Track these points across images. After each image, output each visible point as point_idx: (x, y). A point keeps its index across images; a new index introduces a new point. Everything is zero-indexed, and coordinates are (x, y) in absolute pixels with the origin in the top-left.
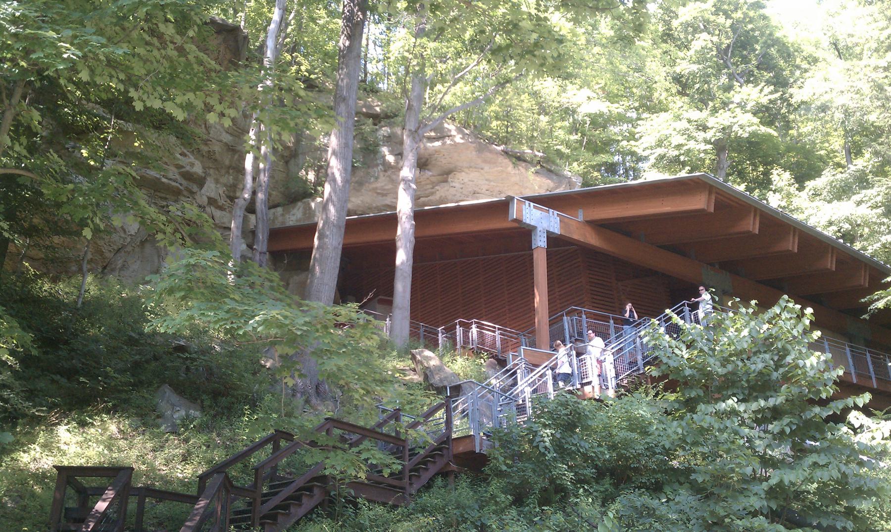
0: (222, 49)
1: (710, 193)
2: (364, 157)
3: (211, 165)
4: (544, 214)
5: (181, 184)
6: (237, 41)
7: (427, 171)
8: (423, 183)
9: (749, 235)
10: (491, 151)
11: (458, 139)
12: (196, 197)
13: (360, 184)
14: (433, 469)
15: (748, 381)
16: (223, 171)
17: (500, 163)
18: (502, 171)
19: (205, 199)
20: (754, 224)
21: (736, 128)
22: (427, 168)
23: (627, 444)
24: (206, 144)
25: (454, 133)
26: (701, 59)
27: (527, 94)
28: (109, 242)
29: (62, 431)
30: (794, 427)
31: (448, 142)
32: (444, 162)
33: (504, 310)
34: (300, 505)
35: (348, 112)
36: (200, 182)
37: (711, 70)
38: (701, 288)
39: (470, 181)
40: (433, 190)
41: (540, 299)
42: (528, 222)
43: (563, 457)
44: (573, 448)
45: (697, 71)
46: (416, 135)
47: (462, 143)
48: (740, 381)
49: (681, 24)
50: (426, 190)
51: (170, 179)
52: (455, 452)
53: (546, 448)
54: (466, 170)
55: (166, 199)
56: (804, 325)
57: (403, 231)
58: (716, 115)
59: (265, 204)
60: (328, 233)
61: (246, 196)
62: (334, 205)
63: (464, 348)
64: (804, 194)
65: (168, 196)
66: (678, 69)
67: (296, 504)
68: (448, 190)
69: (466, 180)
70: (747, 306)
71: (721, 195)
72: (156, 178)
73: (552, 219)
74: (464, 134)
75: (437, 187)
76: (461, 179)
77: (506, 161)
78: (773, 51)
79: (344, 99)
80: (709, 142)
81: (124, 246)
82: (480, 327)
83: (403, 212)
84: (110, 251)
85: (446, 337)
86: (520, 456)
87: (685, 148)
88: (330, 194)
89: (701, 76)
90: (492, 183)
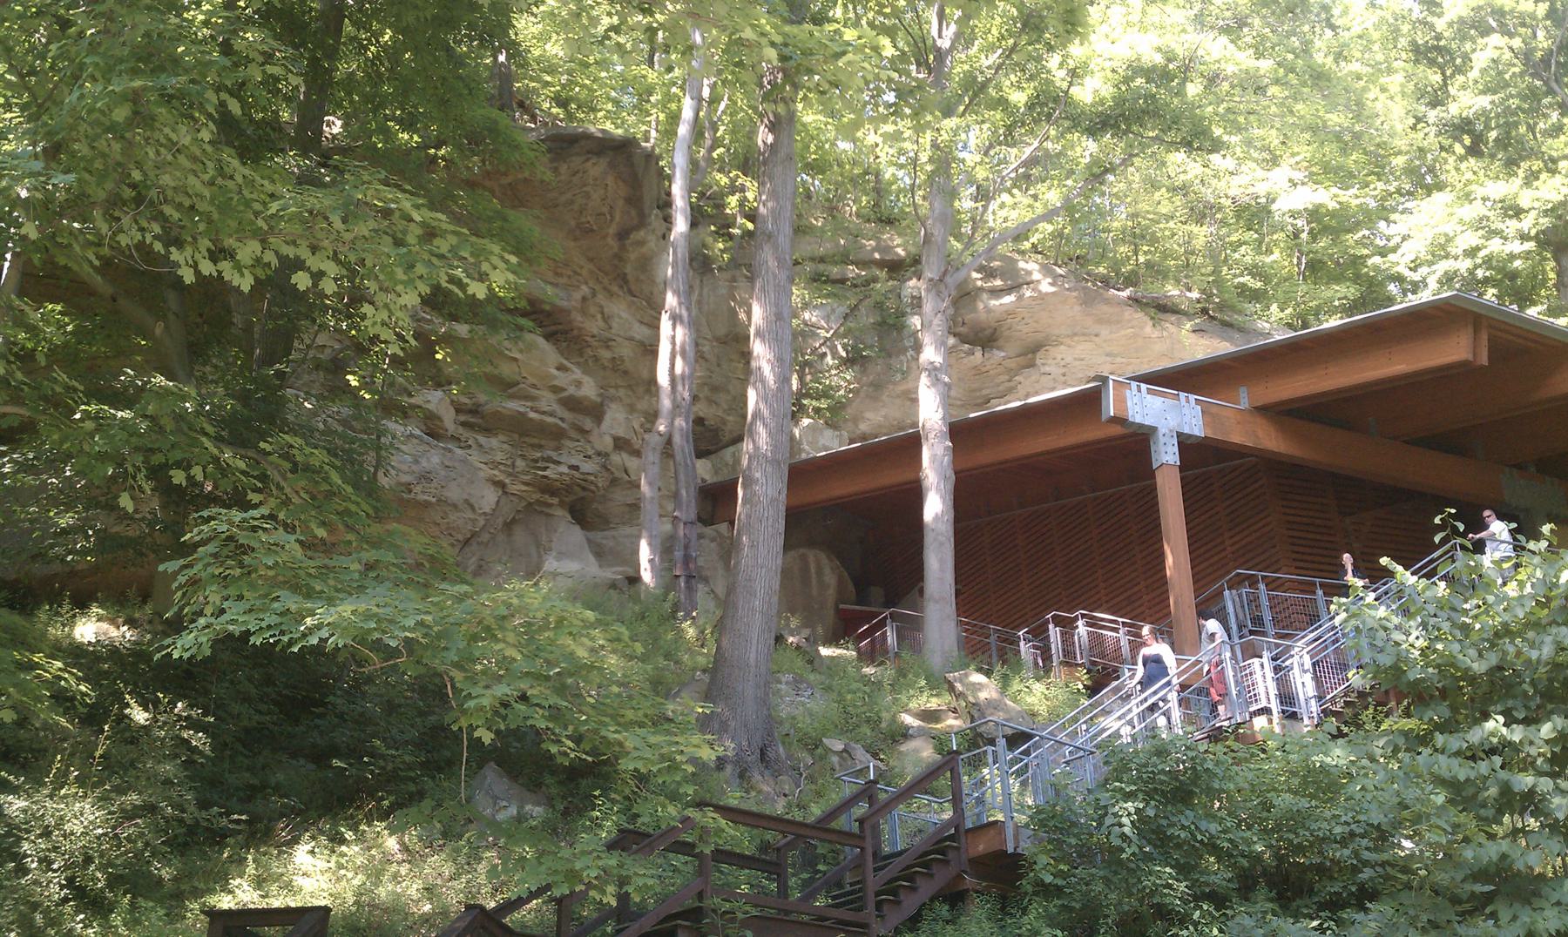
1: (1476, 332)
2: (880, 338)
3: (619, 382)
4: (1169, 402)
5: (562, 419)
7: (995, 352)
10: (1107, 301)
11: (1046, 286)
12: (591, 439)
13: (877, 386)
14: (926, 889)
15: (1533, 683)
16: (641, 390)
17: (1129, 321)
18: (1135, 336)
19: (609, 441)
22: (995, 344)
23: (1297, 819)
24: (608, 347)
25: (1036, 276)
26: (1495, 83)
27: (1164, 190)
28: (448, 529)
31: (1028, 294)
32: (1025, 331)
36: (596, 412)
38: (1487, 513)
40: (1012, 384)
41: (1175, 559)
42: (1138, 419)
43: (1166, 852)
45: (1489, 107)
46: (942, 287)
47: (1053, 293)
48: (1520, 684)
49: (1450, 25)
50: (998, 385)
51: (544, 413)
53: (1124, 836)
54: (1068, 341)
55: (540, 447)
58: (1536, 184)
60: (758, 475)
61: (662, 428)
62: (765, 426)
65: (543, 442)
66: (1454, 110)
69: (1069, 359)
72: (520, 413)
73: (1186, 411)
74: (1056, 277)
76: (1059, 357)
77: (1140, 316)
79: (770, 236)
80: (1524, 237)
81: (474, 534)
82: (1093, 623)
85: (1034, 647)
86: (1086, 854)
87: (1482, 254)
88: (757, 403)
89: (1498, 116)
90: (1119, 360)
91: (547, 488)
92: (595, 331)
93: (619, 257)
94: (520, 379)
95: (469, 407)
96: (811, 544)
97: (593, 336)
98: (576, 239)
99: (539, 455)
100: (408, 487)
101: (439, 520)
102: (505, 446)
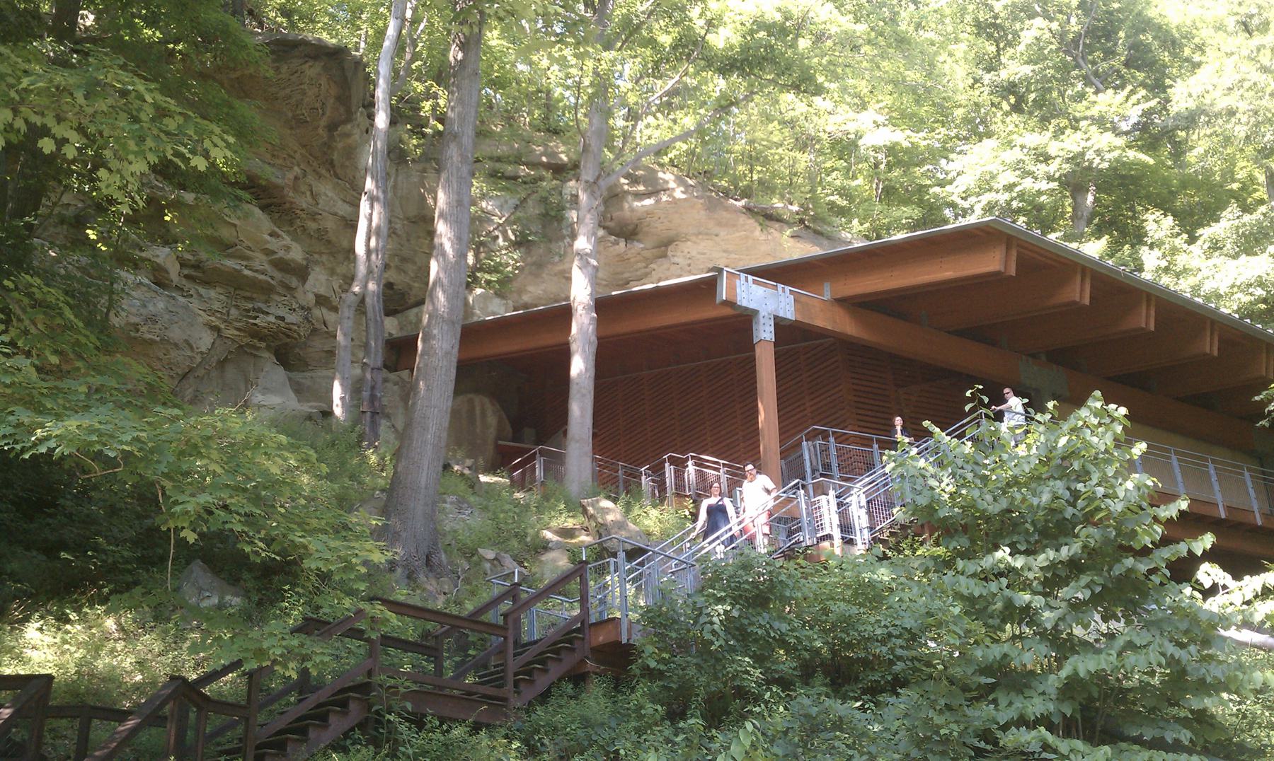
0: (323, 81)
1: (1008, 248)
2: (544, 227)
5: (272, 278)
6: (343, 69)
7: (636, 243)
8: (632, 260)
9: (1074, 309)
10: (727, 209)
11: (679, 194)
12: (296, 295)
13: (540, 265)
14: (555, 671)
18: (747, 237)
20: (1082, 291)
21: (1090, 155)
22: (637, 237)
23: (848, 623)
24: (314, 220)
25: (672, 185)
27: (776, 122)
29: (32, 632)
30: (1098, 589)
31: (664, 198)
33: (736, 437)
34: (326, 727)
35: (461, 155)
36: (302, 273)
37: (1052, 71)
38: (1006, 390)
39: (699, 253)
40: (647, 270)
41: (767, 414)
42: (744, 303)
44: (760, 632)
45: (1031, 74)
46: (596, 188)
47: (685, 199)
48: (1024, 523)
51: (256, 271)
52: (594, 644)
53: (714, 632)
54: (694, 238)
55: (251, 299)
56: (1115, 433)
57: (580, 329)
58: (1062, 137)
59: (378, 297)
60: (435, 332)
62: (444, 292)
63: (678, 495)
64: (1195, 248)
65: (255, 296)
66: (1004, 75)
67: (318, 726)
68: (668, 269)
69: (694, 253)
70: (1043, 410)
71: (1026, 248)
73: (782, 299)
74: (687, 186)
75: (652, 266)
76: (686, 251)
77: (751, 222)
78: (1147, 38)
80: (1050, 178)
81: (191, 370)
82: (700, 463)
83: (578, 300)
84: (172, 377)
85: (653, 481)
86: (683, 645)
87: (1017, 189)
88: (438, 273)
89: (1037, 81)
90: (733, 256)
91: (256, 333)
92: (304, 206)
93: (328, 146)
94: (237, 241)
95: (193, 262)
96: (477, 391)
97: (303, 210)
98: (291, 128)
99: (251, 306)
100: (136, 327)
101: (161, 356)
102: (222, 297)
